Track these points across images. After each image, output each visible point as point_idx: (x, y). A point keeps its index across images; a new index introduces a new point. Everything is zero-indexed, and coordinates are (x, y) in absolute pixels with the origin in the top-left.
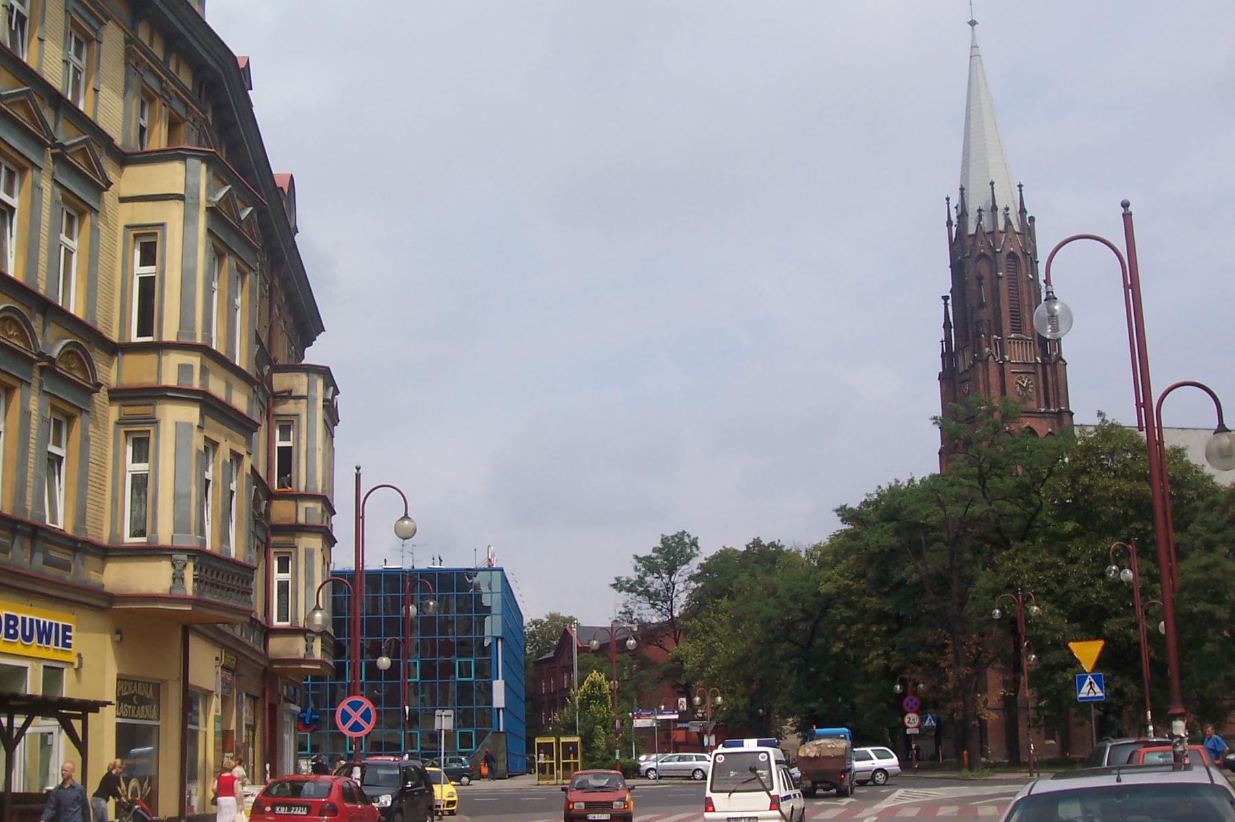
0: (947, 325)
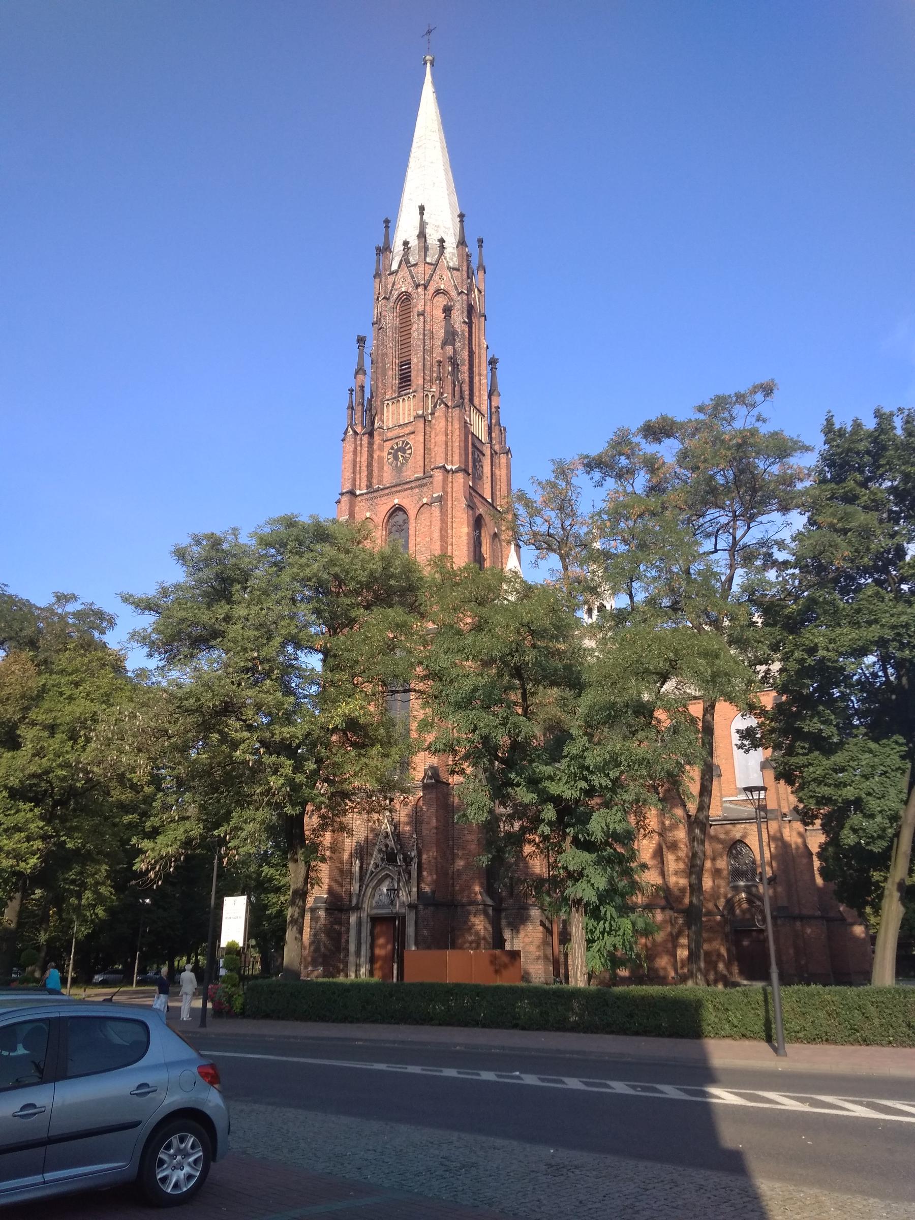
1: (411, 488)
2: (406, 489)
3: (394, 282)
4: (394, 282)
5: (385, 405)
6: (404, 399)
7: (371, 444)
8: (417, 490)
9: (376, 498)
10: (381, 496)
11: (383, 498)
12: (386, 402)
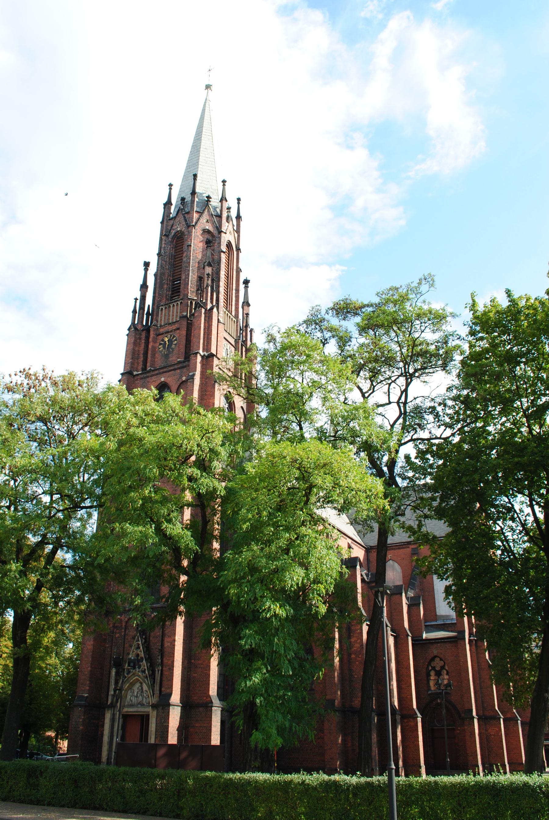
0: (144, 287)
1: (174, 370)
2: (171, 370)
3: (173, 225)
4: (173, 225)
5: (160, 309)
6: (174, 305)
7: (147, 338)
8: (178, 371)
9: (148, 377)
10: (152, 376)
11: (153, 377)
12: (161, 307)
